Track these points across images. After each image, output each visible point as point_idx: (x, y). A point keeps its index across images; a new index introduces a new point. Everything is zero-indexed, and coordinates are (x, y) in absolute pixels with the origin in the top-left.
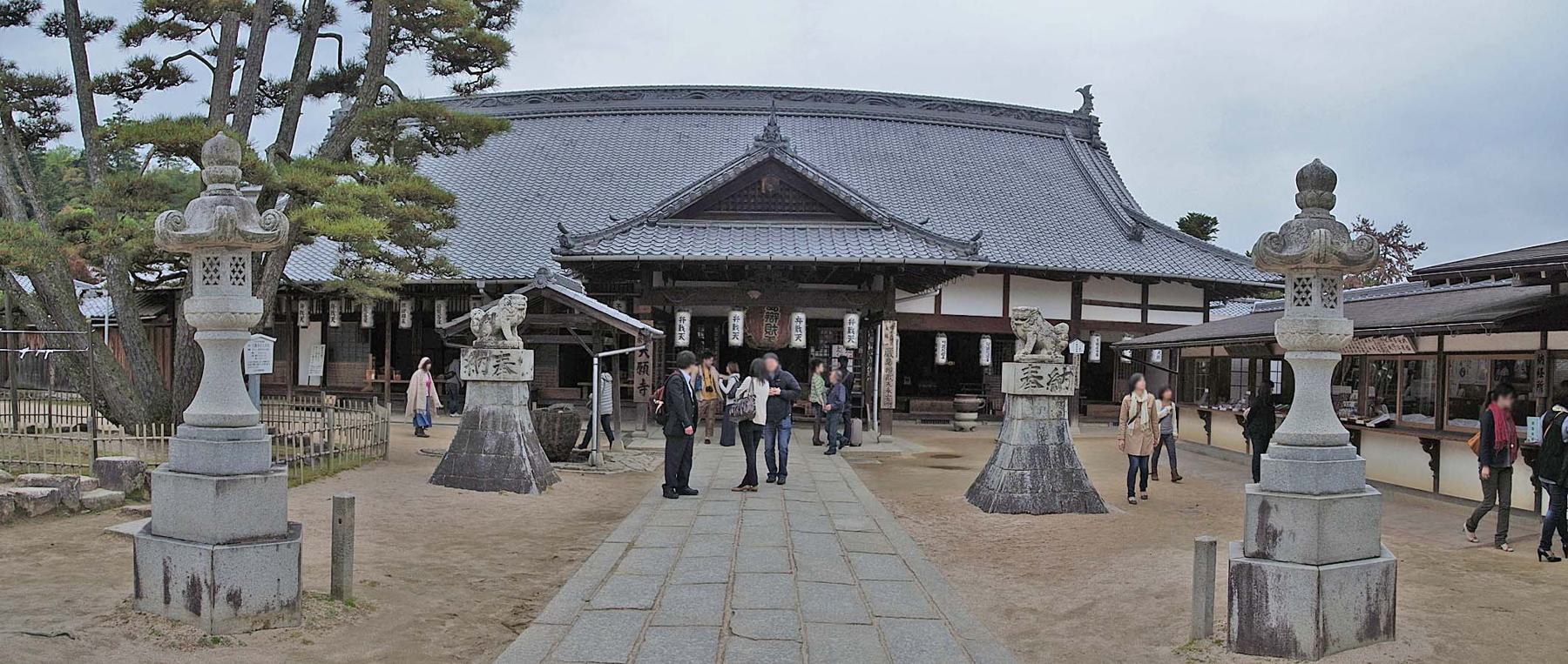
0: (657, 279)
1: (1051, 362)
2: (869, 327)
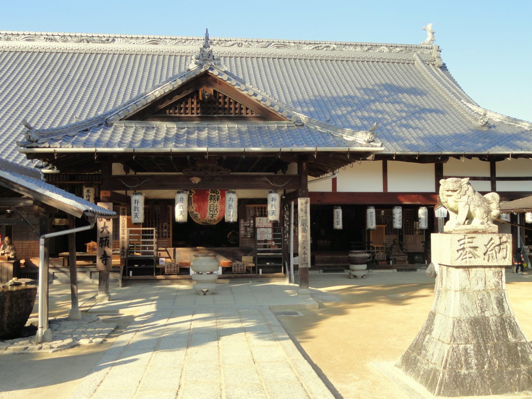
0: (117, 169)
1: (484, 232)
2: (287, 202)
